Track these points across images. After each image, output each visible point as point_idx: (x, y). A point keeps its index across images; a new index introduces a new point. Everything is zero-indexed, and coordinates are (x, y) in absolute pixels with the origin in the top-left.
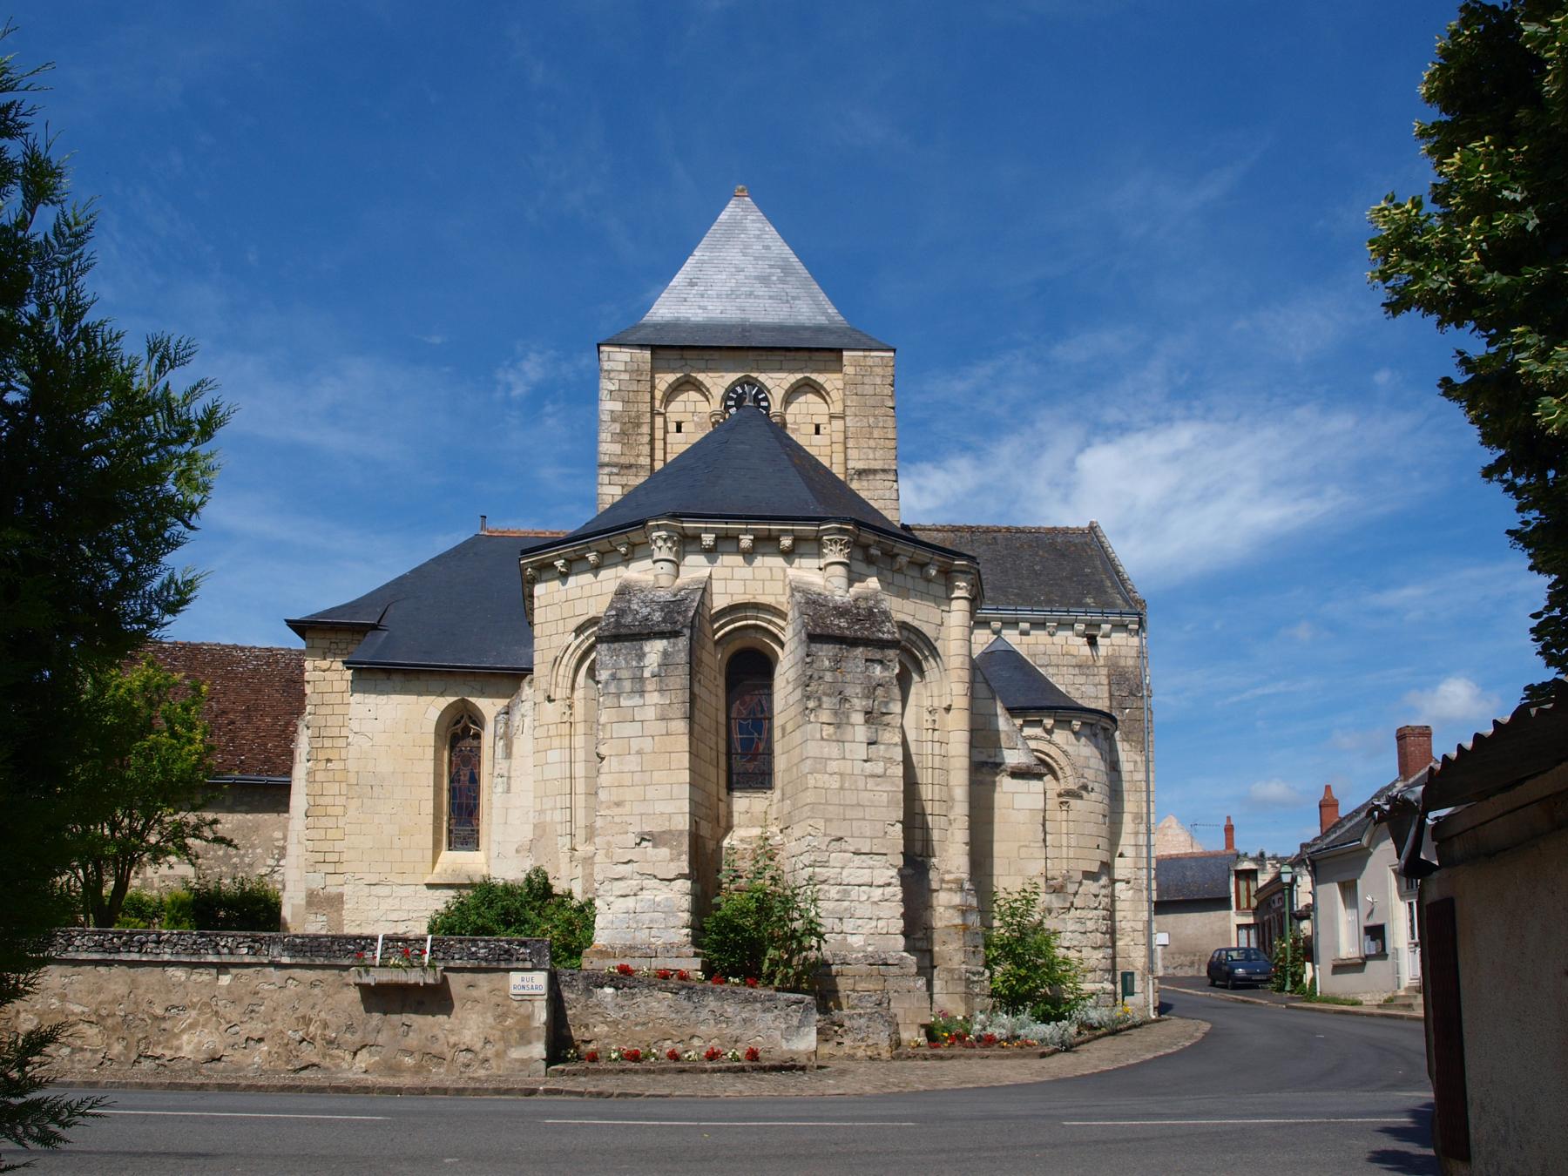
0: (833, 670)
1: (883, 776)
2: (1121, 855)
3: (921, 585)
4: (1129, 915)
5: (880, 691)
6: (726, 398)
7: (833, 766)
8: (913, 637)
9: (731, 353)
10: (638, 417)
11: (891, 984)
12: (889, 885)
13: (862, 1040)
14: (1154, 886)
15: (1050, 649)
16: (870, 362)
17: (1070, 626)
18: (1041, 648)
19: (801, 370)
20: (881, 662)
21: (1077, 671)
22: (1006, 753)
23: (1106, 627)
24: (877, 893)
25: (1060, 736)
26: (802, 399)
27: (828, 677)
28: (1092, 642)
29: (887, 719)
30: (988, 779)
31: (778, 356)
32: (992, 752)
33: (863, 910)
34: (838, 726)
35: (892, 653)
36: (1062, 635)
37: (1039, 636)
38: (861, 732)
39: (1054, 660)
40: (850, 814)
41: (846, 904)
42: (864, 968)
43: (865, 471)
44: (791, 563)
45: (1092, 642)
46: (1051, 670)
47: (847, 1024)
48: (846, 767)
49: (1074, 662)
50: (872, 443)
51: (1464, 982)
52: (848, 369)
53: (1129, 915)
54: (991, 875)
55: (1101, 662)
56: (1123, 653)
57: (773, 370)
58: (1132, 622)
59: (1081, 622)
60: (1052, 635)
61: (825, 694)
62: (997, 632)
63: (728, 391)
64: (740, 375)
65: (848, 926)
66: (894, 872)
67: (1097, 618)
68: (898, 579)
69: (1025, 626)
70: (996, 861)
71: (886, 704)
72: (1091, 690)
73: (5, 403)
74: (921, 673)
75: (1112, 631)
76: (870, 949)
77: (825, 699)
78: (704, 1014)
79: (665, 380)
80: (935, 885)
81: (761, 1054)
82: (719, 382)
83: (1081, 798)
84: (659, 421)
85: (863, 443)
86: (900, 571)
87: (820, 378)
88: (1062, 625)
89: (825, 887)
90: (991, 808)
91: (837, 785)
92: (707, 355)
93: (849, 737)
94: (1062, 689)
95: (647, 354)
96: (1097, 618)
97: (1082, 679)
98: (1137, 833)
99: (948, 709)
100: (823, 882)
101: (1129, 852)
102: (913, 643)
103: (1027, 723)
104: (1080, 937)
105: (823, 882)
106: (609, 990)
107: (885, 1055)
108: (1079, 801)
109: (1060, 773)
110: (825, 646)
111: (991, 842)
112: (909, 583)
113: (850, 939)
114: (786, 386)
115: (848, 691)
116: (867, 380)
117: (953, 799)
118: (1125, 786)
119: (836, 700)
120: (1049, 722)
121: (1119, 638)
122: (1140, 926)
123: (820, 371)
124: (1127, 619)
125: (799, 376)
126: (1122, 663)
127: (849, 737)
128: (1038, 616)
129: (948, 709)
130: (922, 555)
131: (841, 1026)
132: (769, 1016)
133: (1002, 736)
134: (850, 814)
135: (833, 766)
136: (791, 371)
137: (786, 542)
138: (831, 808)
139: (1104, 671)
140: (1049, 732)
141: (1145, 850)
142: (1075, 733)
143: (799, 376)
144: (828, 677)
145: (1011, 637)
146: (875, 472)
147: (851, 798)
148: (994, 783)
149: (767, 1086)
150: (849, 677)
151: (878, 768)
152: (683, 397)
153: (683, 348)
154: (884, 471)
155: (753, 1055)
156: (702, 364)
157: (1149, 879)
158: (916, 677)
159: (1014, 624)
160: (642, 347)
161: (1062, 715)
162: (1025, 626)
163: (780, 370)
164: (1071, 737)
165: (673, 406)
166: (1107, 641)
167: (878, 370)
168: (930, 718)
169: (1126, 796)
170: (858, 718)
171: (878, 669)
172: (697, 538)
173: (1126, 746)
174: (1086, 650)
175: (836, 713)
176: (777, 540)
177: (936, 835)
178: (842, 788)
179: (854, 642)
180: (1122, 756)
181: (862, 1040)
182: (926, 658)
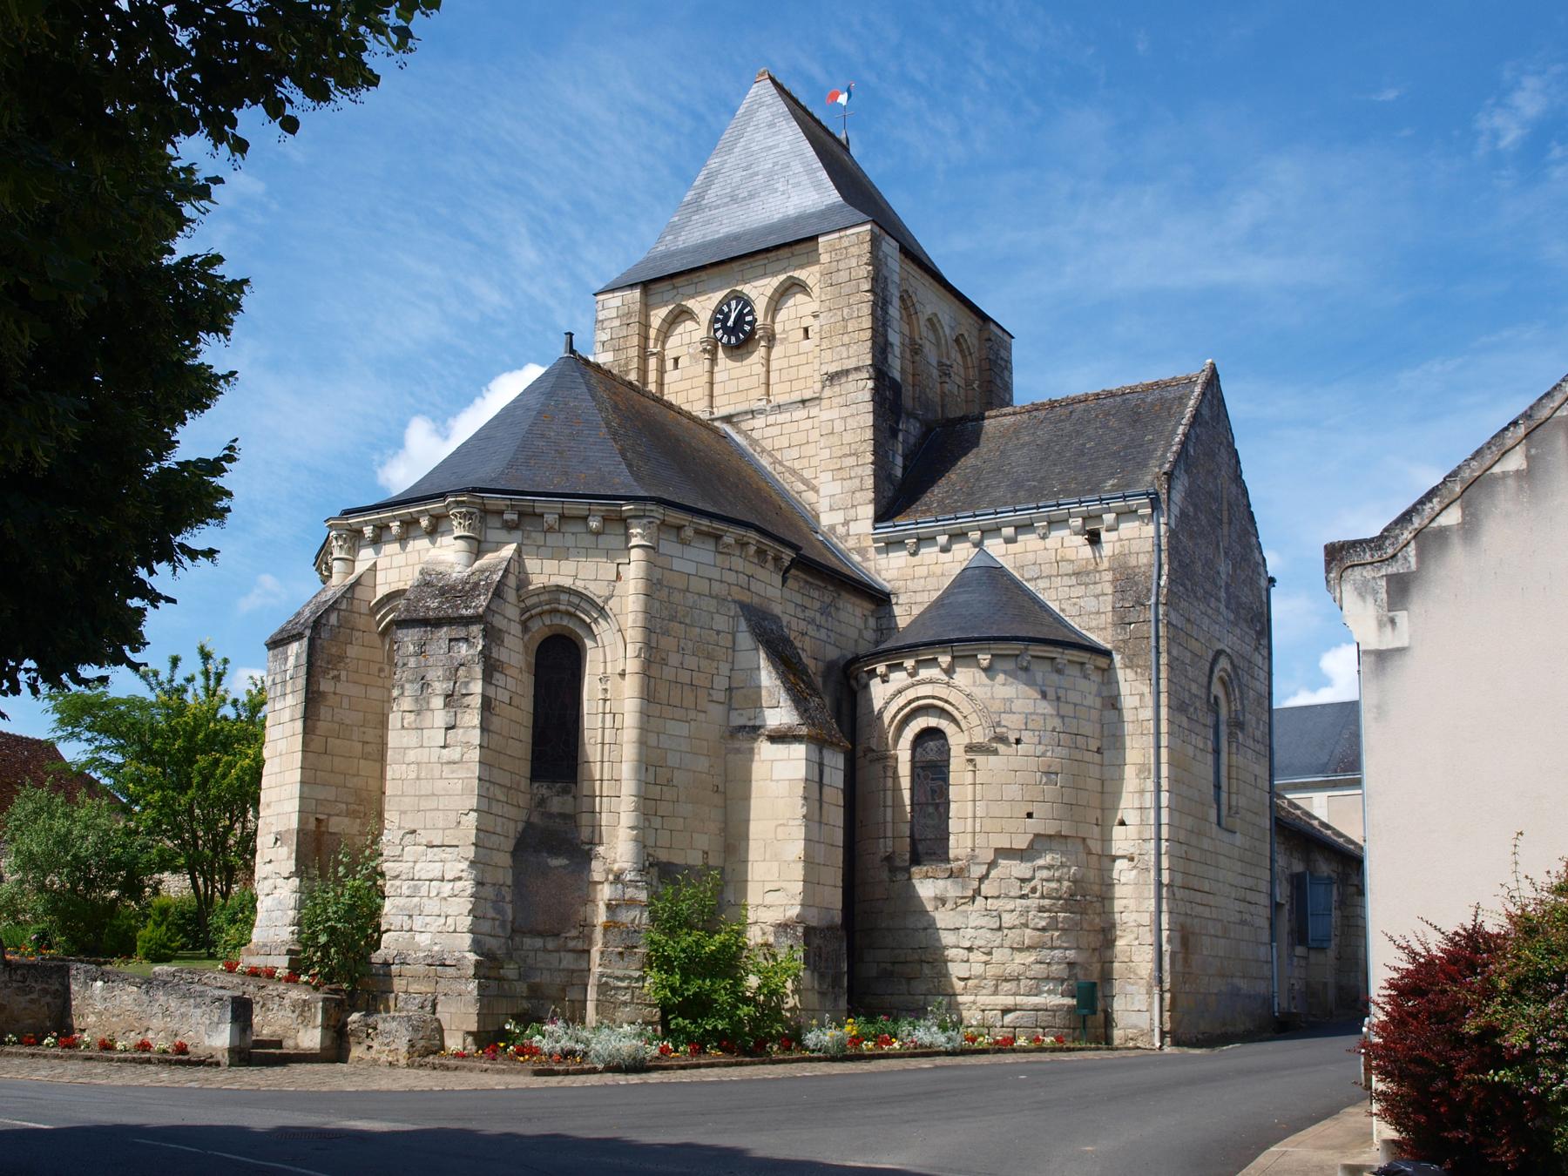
0: (416, 655)
1: (460, 762)
2: (1122, 823)
3: (588, 540)
4: (1132, 904)
5: (461, 672)
6: (714, 320)
7: (412, 755)
8: (576, 600)
9: (715, 270)
10: (627, 364)
11: (442, 987)
12: (460, 879)
13: (388, 1044)
14: (1165, 863)
15: (1043, 557)
16: (845, 243)
17: (1061, 523)
18: (1031, 557)
19: (784, 270)
20: (466, 640)
21: (1073, 580)
22: (767, 712)
23: (1109, 518)
24: (447, 888)
25: (963, 676)
26: (791, 302)
27: (412, 662)
28: (1094, 538)
29: (467, 700)
30: (746, 745)
31: (761, 260)
32: (751, 713)
33: (432, 906)
34: (418, 713)
35: (476, 629)
36: (1056, 535)
37: (1029, 541)
38: (440, 717)
39: (1046, 570)
40: (424, 804)
41: (416, 900)
42: (421, 969)
43: (837, 373)
44: (433, 543)
45: (1094, 538)
46: (1042, 584)
47: (380, 1027)
48: (423, 755)
49: (1069, 568)
50: (846, 339)
51: (1297, 1042)
52: (824, 258)
53: (1132, 904)
54: (746, 861)
55: (1106, 565)
56: (1134, 549)
57: (757, 278)
58: (1141, 506)
59: (1076, 515)
60: (1044, 537)
61: (408, 681)
62: (978, 544)
63: (715, 312)
64: (726, 291)
65: (418, 923)
66: (465, 865)
67: (1095, 507)
68: (552, 539)
69: (1008, 531)
70: (752, 845)
71: (467, 684)
72: (1090, 604)
73: (404, 425)
74: (594, 637)
75: (1016, 534)
76: (436, 948)
77: (407, 686)
78: (156, 1009)
79: (658, 316)
80: (597, 877)
81: (190, 1049)
82: (704, 305)
83: (995, 752)
84: (653, 363)
85: (837, 341)
86: (550, 530)
87: (801, 274)
88: (1053, 524)
89: (397, 883)
90: (747, 781)
91: (413, 775)
92: (694, 277)
93: (427, 724)
94: (1055, 606)
95: (636, 293)
96: (1095, 507)
97: (1080, 591)
98: (1142, 792)
99: (623, 675)
100: (396, 877)
101: (1131, 817)
102: (577, 607)
103: (921, 664)
104: (989, 935)
105: (396, 877)
106: (99, 983)
107: (403, 1062)
108: (992, 758)
109: (963, 723)
110: (411, 631)
111: (748, 821)
112: (570, 540)
113: (418, 937)
114: (769, 292)
115: (431, 675)
116: (842, 265)
117: (1229, 726)
118: (1128, 728)
119: (417, 686)
120: (945, 660)
121: (1129, 528)
122: (1146, 919)
123: (802, 267)
124: (1133, 503)
125: (782, 277)
126: (1133, 562)
127: (427, 724)
128: (1022, 517)
129: (623, 675)
130: (575, 507)
131: (375, 1028)
132: (199, 1011)
133: (764, 693)
134: (424, 804)
135: (412, 755)
136: (775, 274)
137: (424, 522)
138: (406, 799)
139: (1108, 576)
140: (949, 672)
141: (1152, 814)
142: (985, 670)
143: (782, 277)
144: (412, 662)
145: (995, 547)
146: (846, 372)
147: (426, 787)
148: (751, 751)
149: (925, 1063)
150: (431, 661)
151: (453, 754)
152: (680, 329)
153: (672, 276)
154: (857, 369)
155: (182, 1049)
156: (691, 290)
157: (1159, 854)
158: (589, 643)
159: (995, 531)
160: (632, 286)
161: (960, 649)
162: (1008, 531)
163: (765, 275)
164: (981, 677)
165: (671, 342)
166: (1113, 535)
167: (854, 250)
168: (600, 687)
169: (1128, 742)
170: (438, 702)
171: (464, 647)
172: (360, 532)
173: (1130, 674)
174: (1087, 551)
175: (417, 700)
176: (418, 522)
177: (605, 819)
178: (418, 778)
179: (437, 623)
180: (1124, 689)
181: (388, 1044)
182: (595, 621)
